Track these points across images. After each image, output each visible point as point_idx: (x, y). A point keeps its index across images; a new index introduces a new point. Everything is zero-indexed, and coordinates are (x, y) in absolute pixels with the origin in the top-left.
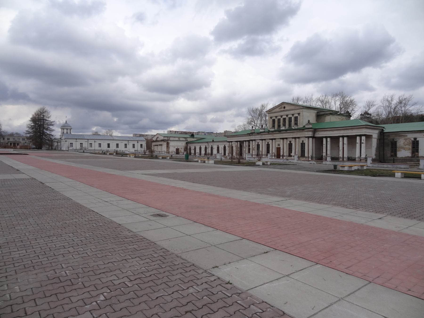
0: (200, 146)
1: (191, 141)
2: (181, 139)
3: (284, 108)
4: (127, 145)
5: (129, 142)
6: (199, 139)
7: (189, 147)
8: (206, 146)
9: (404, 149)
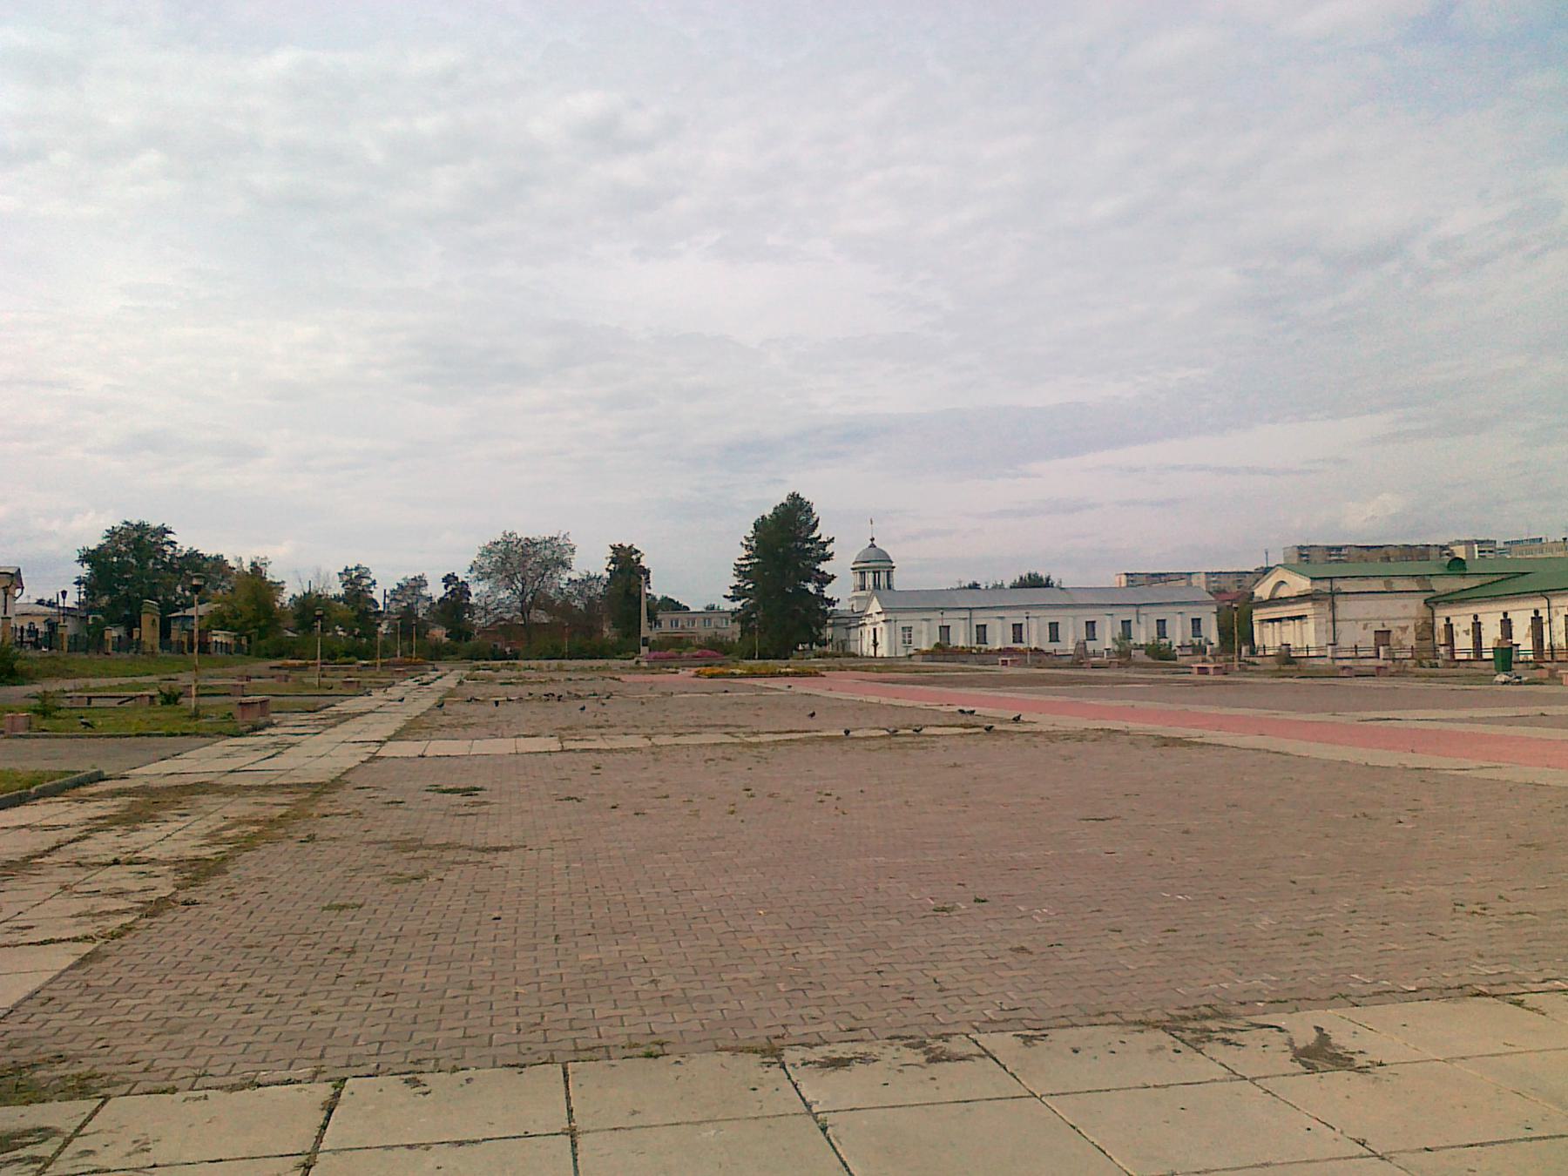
0: (1505, 614)
1: (1453, 593)
2: (1399, 585)
4: (1133, 624)
6: (1495, 578)
7: (1440, 624)
8: (1536, 612)
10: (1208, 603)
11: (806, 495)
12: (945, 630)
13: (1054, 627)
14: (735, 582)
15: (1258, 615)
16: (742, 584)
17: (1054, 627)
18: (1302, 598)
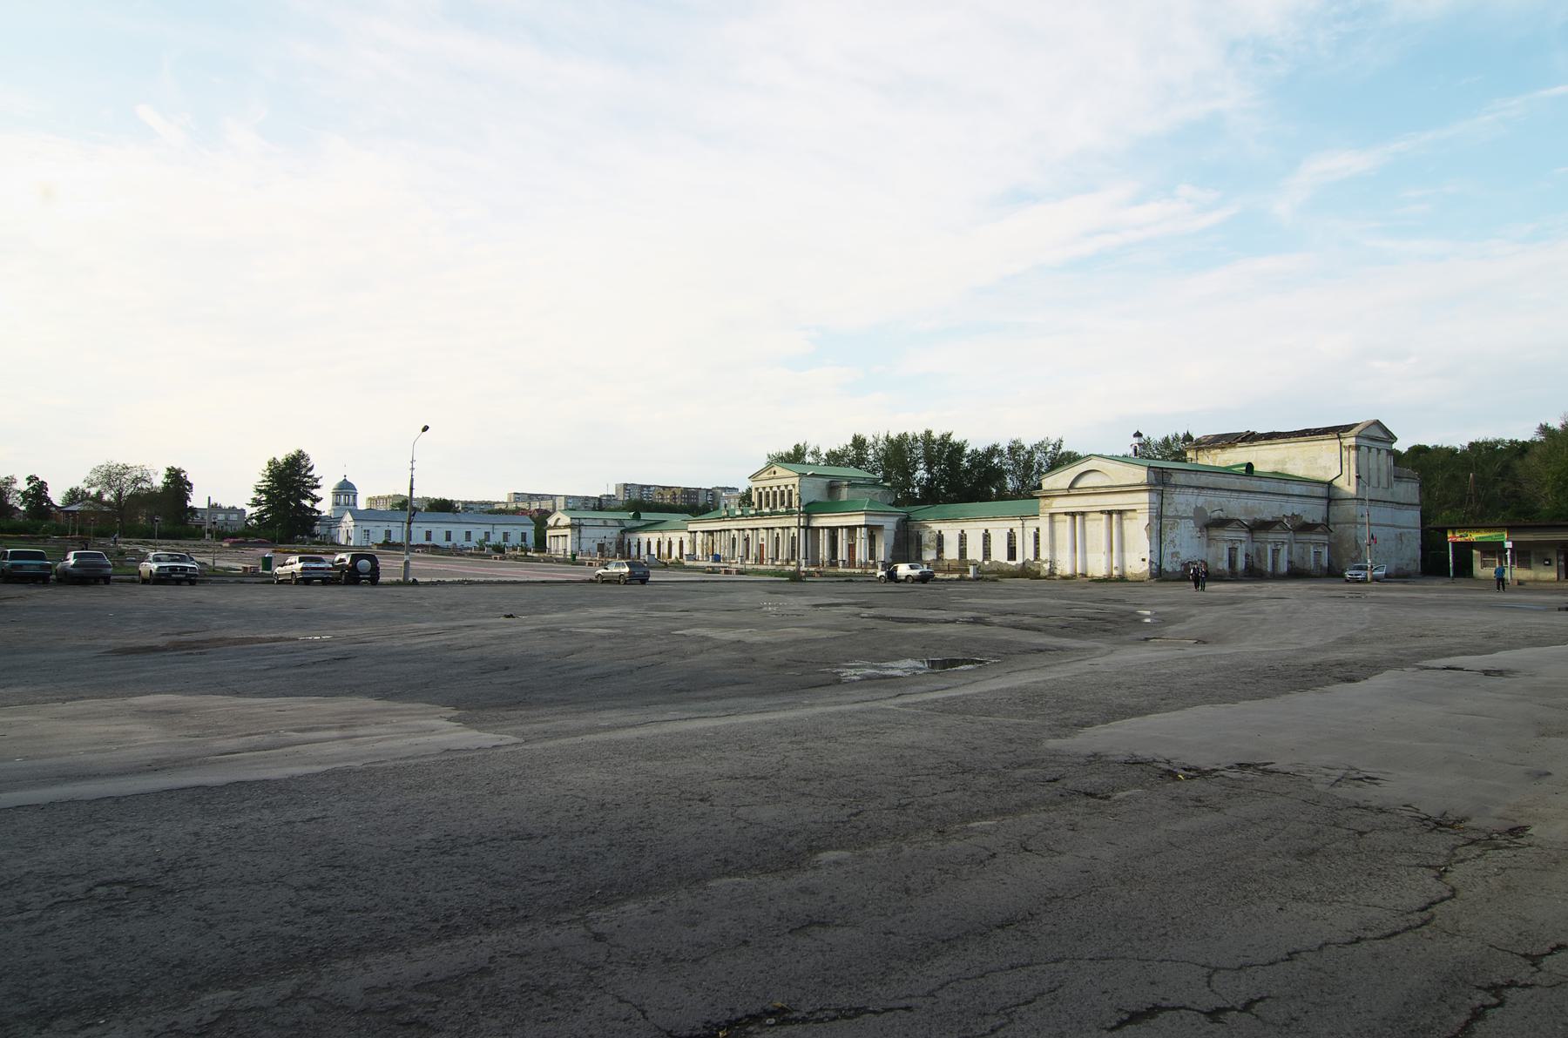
3: (775, 473)
5: (496, 527)
9: (929, 547)
10: (532, 525)
11: (306, 451)
12: (388, 533)
13: (468, 534)
14: (254, 495)
15: (549, 533)
16: (259, 497)
17: (468, 534)
18: (566, 527)
